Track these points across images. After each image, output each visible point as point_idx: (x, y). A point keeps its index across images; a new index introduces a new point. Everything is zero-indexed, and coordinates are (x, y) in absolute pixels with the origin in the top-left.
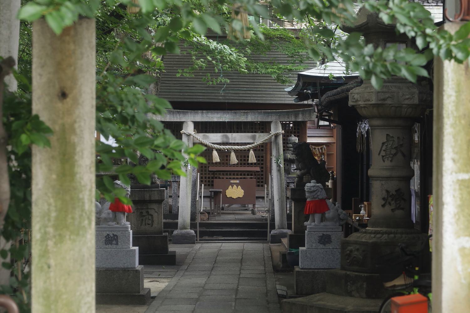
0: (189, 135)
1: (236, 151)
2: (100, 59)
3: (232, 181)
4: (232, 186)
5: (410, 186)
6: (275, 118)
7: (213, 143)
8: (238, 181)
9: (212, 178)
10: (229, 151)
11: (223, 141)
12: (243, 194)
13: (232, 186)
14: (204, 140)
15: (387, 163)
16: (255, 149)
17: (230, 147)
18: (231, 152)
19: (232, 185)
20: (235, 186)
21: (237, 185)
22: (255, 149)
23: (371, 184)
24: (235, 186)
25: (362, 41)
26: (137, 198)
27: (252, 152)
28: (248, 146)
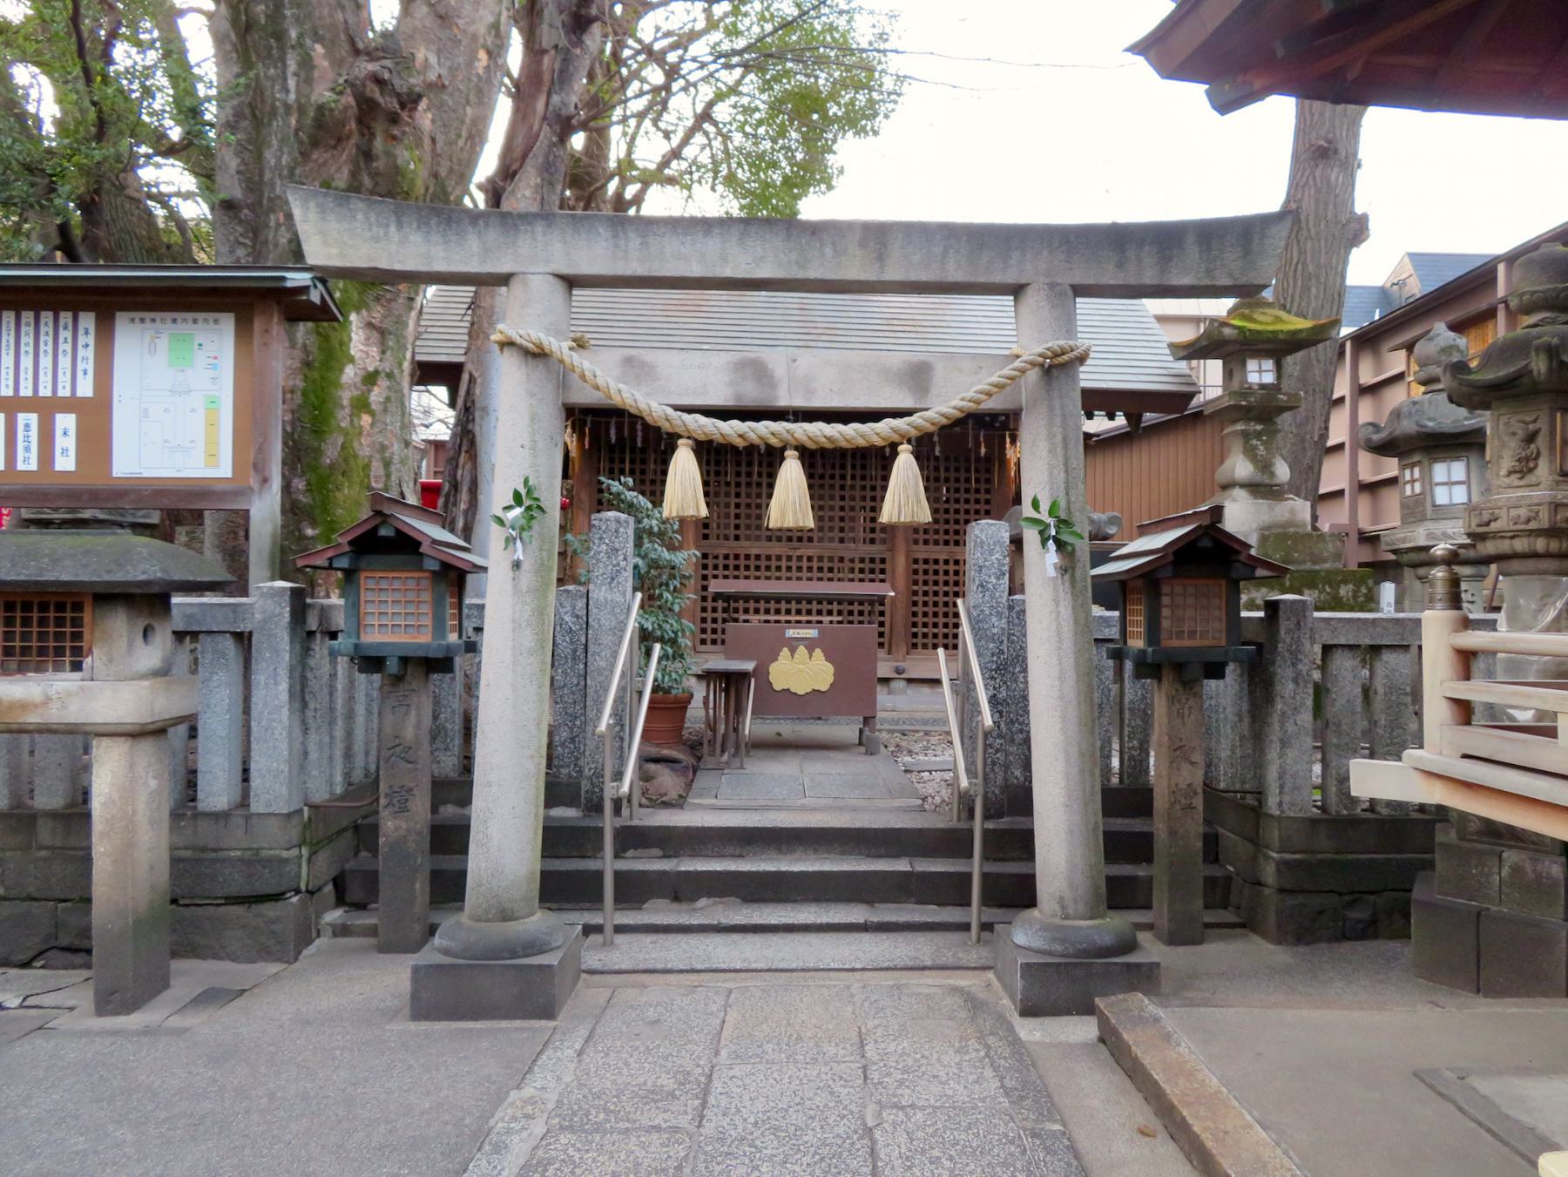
0: (536, 355)
1: (816, 460)
2: (633, 57)
3: (791, 633)
4: (793, 651)
5: (710, 895)
6: (1042, 266)
7: (677, 408)
8: (812, 633)
9: (724, 621)
10: (771, 457)
11: (738, 396)
12: (830, 679)
13: (793, 651)
14: (621, 386)
15: (520, 243)
16: (923, 446)
17: (780, 427)
18: (672, 448)
19: (792, 645)
20: (802, 650)
21: (811, 645)
22: (923, 446)
23: (147, 633)
24: (802, 650)
25: (1445, 371)
26: (1440, 574)
27: (905, 467)
28: (885, 427)
